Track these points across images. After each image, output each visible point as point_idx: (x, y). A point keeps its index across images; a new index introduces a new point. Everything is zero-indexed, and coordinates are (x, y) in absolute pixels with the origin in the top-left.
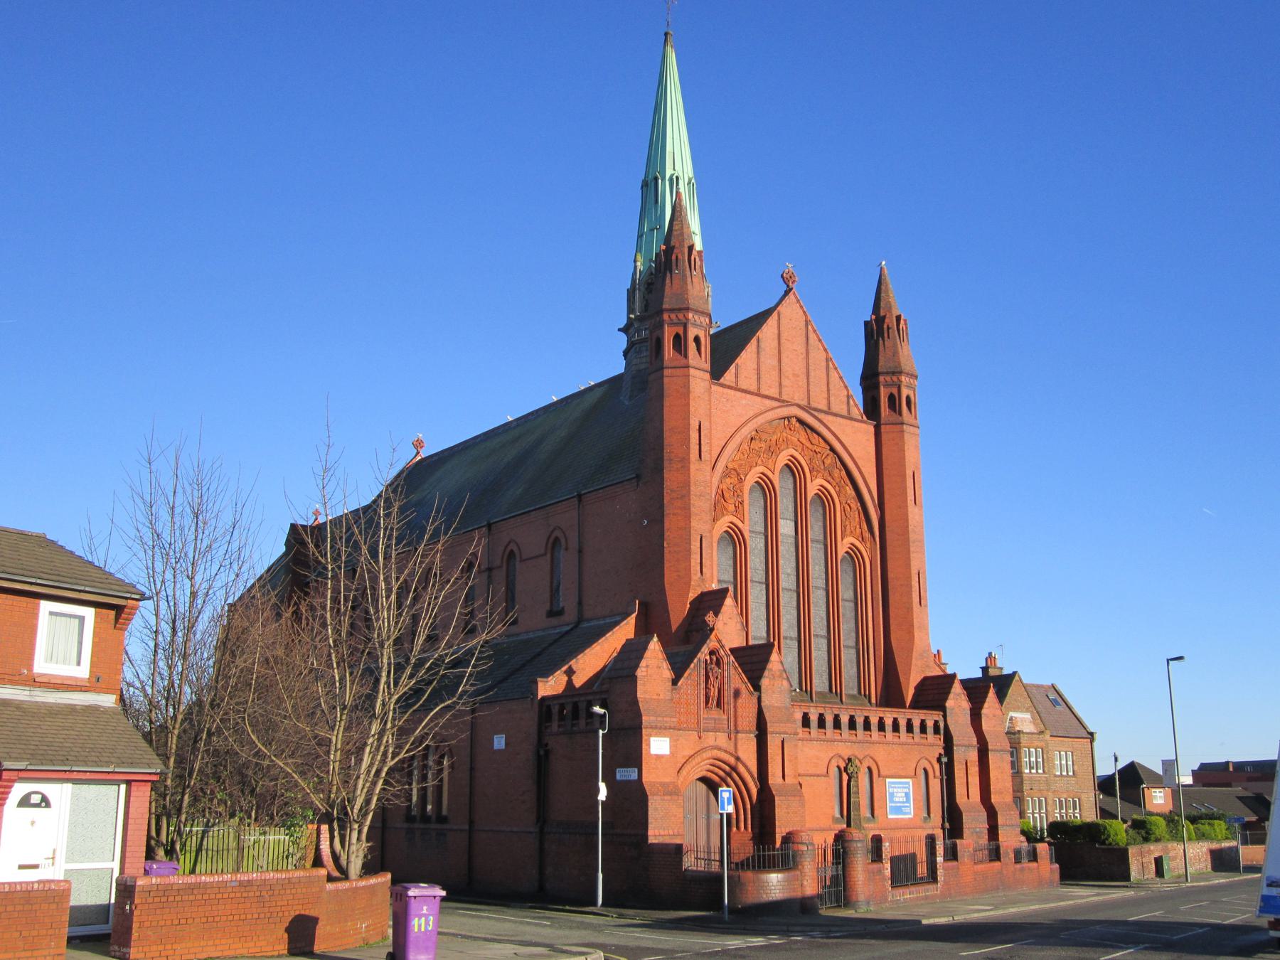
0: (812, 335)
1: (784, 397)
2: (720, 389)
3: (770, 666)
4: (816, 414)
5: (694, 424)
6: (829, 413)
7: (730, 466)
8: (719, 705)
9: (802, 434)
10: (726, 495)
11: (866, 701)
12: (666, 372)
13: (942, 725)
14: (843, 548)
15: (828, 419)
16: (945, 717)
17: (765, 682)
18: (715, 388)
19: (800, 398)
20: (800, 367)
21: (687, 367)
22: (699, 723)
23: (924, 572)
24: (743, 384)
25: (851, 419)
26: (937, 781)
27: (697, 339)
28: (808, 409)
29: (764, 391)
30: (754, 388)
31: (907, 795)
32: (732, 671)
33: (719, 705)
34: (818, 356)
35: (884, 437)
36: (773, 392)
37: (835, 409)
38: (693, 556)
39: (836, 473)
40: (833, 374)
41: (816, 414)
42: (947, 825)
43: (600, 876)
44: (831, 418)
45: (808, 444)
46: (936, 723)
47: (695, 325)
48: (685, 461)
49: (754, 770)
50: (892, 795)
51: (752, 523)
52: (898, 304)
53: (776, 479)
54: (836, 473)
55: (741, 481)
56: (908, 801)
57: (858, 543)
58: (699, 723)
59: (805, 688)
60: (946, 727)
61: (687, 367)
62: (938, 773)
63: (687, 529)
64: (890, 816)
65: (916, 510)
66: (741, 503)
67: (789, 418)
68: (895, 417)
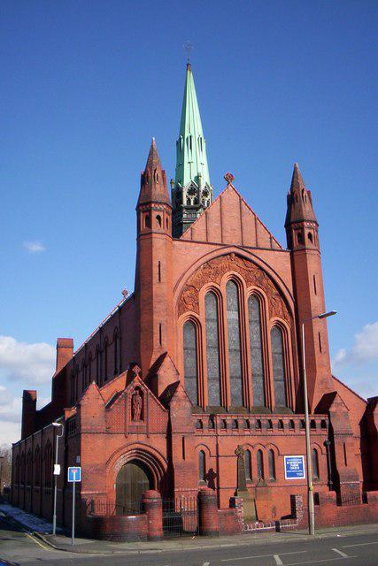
0: (244, 206)
1: (225, 243)
2: (181, 243)
3: (177, 394)
4: (248, 250)
5: (155, 263)
6: (257, 248)
7: (189, 283)
8: (142, 418)
9: (241, 263)
10: (187, 300)
11: (290, 410)
12: (154, 235)
13: (327, 422)
14: (270, 323)
15: (262, 255)
16: (329, 417)
17: (173, 404)
18: (176, 243)
19: (236, 242)
20: (236, 224)
21: (305, 249)
22: (125, 430)
23: (326, 334)
24: (196, 238)
25: (274, 250)
26: (325, 457)
27: (158, 217)
28: (242, 247)
29: (195, 239)
30: (204, 240)
31: (301, 466)
32: (150, 398)
33: (142, 418)
34: (249, 218)
35: (295, 258)
36: (218, 241)
37: (262, 245)
38: (155, 336)
39: (265, 282)
40: (260, 228)
41: (248, 250)
42: (331, 483)
43: (55, 516)
44: (258, 251)
45: (245, 267)
46: (323, 422)
47: (157, 210)
48: (151, 283)
49: (165, 455)
50: (288, 466)
51: (205, 312)
52: (306, 184)
53: (223, 289)
54: (265, 282)
55: (197, 292)
56: (301, 468)
57: (281, 320)
58: (125, 430)
59: (198, 405)
60: (330, 424)
61: (305, 249)
62: (325, 452)
63: (151, 321)
64: (287, 478)
65: (316, 298)
66: (198, 304)
67: (230, 254)
68: (301, 247)
